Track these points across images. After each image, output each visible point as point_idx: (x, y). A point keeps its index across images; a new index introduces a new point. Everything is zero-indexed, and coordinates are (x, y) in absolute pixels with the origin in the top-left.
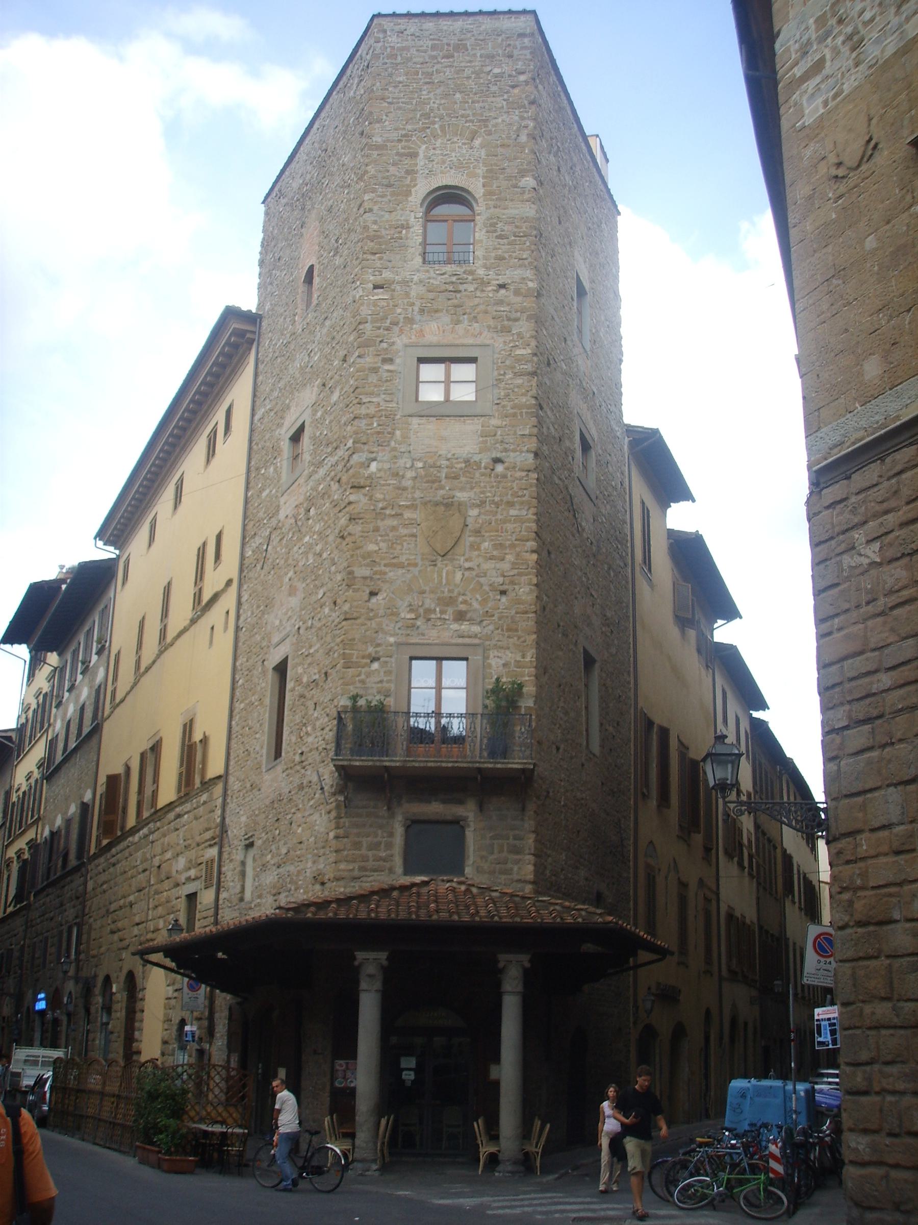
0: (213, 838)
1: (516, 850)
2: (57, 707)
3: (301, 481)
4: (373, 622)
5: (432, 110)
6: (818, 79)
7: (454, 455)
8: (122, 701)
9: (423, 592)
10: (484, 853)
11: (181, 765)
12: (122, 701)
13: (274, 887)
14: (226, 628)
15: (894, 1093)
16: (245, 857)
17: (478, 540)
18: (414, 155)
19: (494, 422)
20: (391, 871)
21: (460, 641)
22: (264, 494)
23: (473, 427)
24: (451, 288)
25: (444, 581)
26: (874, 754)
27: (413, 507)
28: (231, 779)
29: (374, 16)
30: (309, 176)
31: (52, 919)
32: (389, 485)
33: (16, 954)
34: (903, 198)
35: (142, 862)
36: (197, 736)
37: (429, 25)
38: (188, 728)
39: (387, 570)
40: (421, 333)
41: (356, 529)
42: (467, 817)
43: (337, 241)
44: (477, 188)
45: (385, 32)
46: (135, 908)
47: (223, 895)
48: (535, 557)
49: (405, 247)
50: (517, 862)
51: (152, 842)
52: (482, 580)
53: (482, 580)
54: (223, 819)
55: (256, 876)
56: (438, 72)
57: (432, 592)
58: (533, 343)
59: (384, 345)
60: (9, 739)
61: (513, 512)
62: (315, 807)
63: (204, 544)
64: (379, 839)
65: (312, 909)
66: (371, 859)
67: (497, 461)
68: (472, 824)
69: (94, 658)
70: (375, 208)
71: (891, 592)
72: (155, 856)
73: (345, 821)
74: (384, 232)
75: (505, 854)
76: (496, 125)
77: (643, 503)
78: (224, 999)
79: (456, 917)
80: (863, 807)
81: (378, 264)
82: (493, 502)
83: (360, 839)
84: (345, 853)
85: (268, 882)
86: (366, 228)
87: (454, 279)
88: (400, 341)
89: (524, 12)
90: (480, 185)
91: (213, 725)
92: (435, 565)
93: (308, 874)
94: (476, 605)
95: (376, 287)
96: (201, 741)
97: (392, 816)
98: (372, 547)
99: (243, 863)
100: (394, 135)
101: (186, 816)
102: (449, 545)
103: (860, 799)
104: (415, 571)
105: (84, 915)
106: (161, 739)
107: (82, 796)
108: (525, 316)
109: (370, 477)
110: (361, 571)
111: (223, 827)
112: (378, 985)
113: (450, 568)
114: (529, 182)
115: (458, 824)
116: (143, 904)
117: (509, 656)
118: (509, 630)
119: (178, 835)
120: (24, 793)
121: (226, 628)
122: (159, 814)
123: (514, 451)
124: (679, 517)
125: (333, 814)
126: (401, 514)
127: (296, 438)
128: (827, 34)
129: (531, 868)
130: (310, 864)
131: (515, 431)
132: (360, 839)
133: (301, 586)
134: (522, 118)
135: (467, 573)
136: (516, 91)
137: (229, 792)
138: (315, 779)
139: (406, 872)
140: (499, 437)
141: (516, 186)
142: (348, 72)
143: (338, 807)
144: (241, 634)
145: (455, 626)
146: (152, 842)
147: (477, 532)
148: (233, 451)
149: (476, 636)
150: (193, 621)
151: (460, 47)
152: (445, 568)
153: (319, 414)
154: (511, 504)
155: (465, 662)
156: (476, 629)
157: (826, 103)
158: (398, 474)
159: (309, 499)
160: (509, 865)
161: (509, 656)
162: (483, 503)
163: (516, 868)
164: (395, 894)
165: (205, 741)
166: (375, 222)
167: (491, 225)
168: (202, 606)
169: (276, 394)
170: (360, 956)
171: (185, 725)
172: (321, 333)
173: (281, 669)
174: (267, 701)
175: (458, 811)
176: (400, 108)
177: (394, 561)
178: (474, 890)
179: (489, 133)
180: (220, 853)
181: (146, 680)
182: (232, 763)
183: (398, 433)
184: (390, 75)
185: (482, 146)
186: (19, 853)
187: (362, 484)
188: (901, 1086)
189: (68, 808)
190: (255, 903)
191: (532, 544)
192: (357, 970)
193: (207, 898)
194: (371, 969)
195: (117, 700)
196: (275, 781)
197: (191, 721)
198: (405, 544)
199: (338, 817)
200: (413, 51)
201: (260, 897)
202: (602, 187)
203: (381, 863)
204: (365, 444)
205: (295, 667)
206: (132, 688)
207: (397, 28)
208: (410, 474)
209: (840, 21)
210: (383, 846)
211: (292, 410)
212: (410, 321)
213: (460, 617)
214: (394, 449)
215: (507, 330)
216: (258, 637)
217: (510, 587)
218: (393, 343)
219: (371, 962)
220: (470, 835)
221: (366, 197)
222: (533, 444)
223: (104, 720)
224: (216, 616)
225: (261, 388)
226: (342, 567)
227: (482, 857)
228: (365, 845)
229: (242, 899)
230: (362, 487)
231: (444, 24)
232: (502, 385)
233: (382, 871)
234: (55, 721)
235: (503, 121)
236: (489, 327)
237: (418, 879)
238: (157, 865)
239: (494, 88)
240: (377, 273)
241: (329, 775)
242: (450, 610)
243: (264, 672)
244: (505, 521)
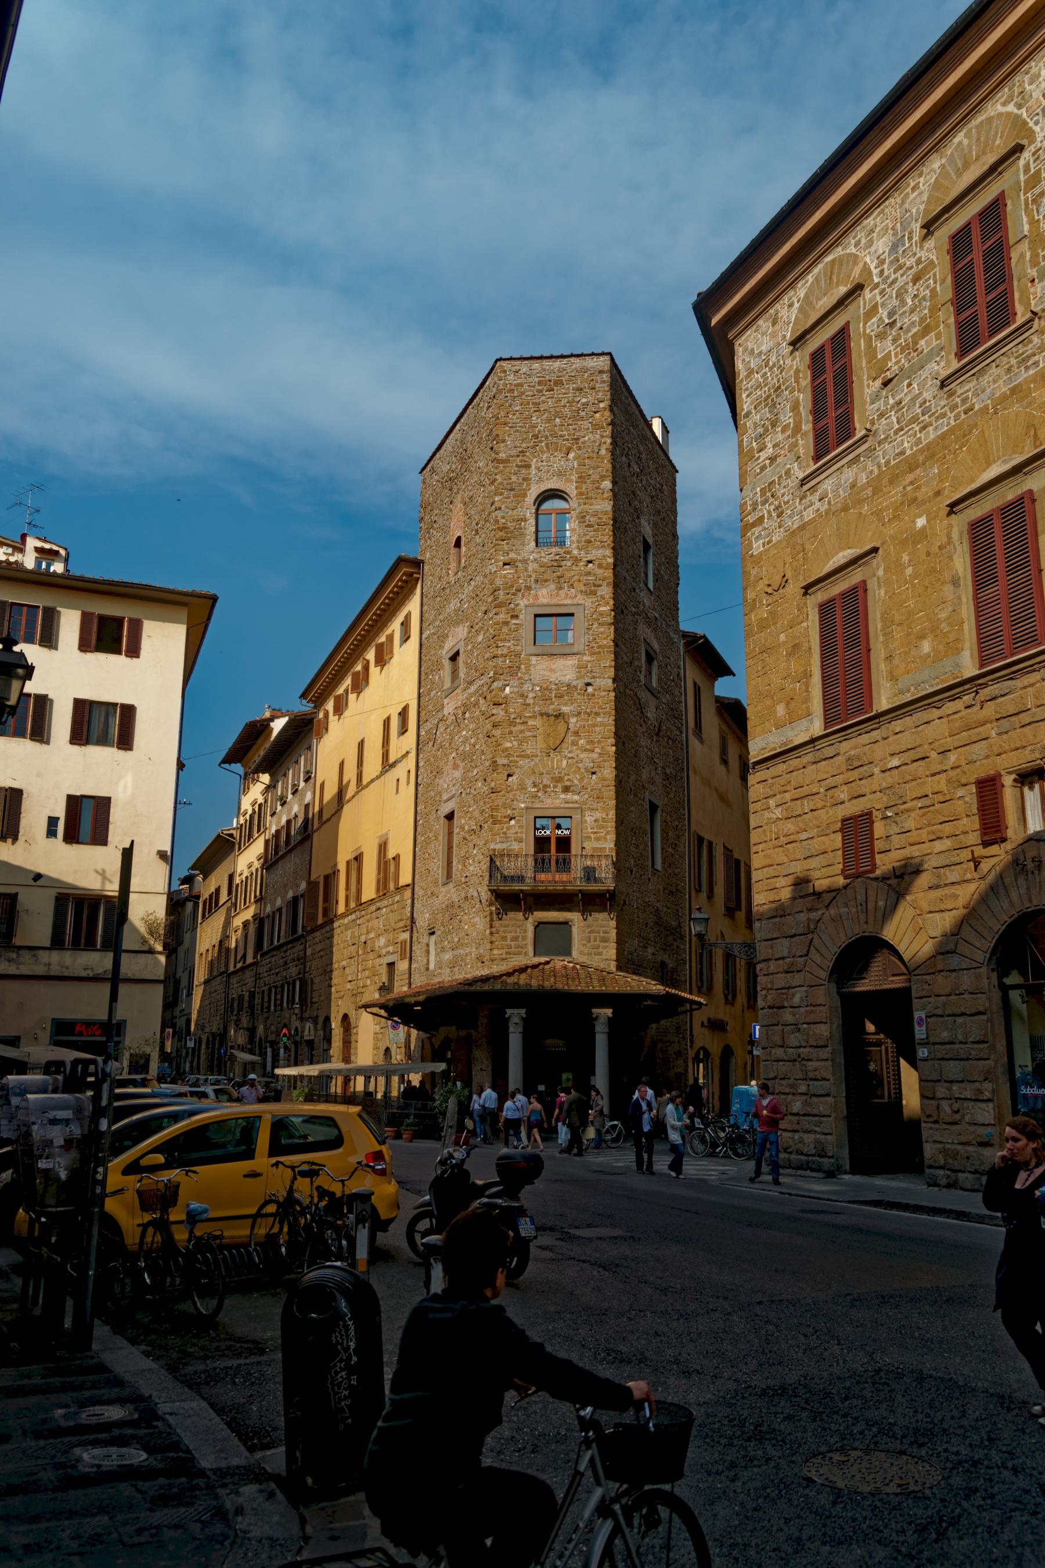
1: (605, 940)
2: (272, 815)
3: (459, 691)
6: (760, 528)
8: (328, 820)
9: (542, 774)
11: (379, 873)
12: (328, 820)
14: (408, 783)
15: (784, 1094)
17: (577, 738)
18: (528, 466)
19: (586, 658)
20: (526, 954)
21: (567, 805)
22: (433, 693)
23: (571, 661)
26: (777, 920)
27: (534, 717)
28: (417, 888)
29: (497, 360)
30: (454, 466)
31: (277, 974)
33: (246, 998)
34: (798, 616)
36: (391, 855)
37: (536, 365)
38: (383, 847)
40: (536, 597)
41: (497, 732)
43: (477, 524)
44: (571, 490)
45: (505, 372)
46: (347, 971)
47: (413, 966)
48: (614, 748)
49: (523, 535)
50: (605, 947)
52: (580, 765)
53: (580, 765)
55: (437, 955)
56: (543, 402)
57: (547, 773)
58: (612, 602)
59: (512, 606)
60: (231, 835)
61: (599, 719)
65: (479, 983)
67: (588, 684)
69: (302, 784)
70: (503, 507)
71: (786, 836)
74: (509, 525)
76: (584, 443)
77: (695, 684)
78: (414, 1032)
79: (566, 987)
80: (772, 947)
81: (506, 548)
82: (586, 713)
86: (497, 521)
88: (523, 603)
89: (603, 354)
90: (574, 487)
91: (402, 846)
94: (576, 782)
95: (505, 564)
96: (394, 859)
98: (508, 745)
99: (428, 945)
100: (514, 452)
102: (558, 742)
103: (770, 943)
104: (537, 760)
105: (305, 972)
107: (298, 886)
108: (605, 583)
109: (506, 697)
110: (501, 761)
112: (520, 1029)
114: (607, 484)
116: (354, 968)
117: (598, 815)
118: (598, 798)
120: (247, 878)
121: (408, 783)
123: (599, 677)
124: (723, 687)
125: (488, 919)
127: (454, 658)
128: (767, 501)
129: (615, 951)
133: (462, 765)
134: (602, 436)
136: (598, 415)
138: (475, 894)
139: (535, 955)
140: (589, 668)
141: (598, 488)
142: (480, 395)
143: (491, 914)
144: (420, 788)
145: (563, 796)
147: (576, 733)
148: (405, 657)
150: (382, 773)
151: (559, 383)
152: (556, 757)
153: (469, 647)
154: (597, 714)
156: (576, 797)
157: (764, 544)
159: (464, 705)
161: (598, 815)
162: (579, 713)
163: (604, 951)
164: (529, 970)
165: (396, 858)
166: (503, 517)
168: (388, 765)
169: (437, 623)
170: (509, 1011)
171: (380, 846)
172: (468, 589)
174: (441, 838)
176: (517, 431)
178: (578, 967)
179: (580, 449)
181: (324, 827)
182: (417, 877)
184: (510, 406)
185: (575, 458)
186: (246, 924)
188: (787, 1090)
189: (287, 893)
191: (612, 741)
192: (507, 1020)
193: (402, 966)
194: (516, 1020)
195: (324, 819)
196: (449, 893)
197: (385, 843)
199: (492, 920)
200: (526, 387)
201: (441, 968)
202: (664, 457)
205: (460, 818)
207: (514, 369)
208: (531, 695)
209: (773, 496)
211: (450, 638)
212: (529, 588)
213: (566, 789)
214: (520, 678)
215: (593, 593)
216: (432, 794)
217: (597, 770)
219: (516, 1016)
221: (496, 499)
222: (612, 674)
223: (313, 832)
224: (400, 771)
225: (426, 615)
226: (488, 757)
229: (427, 969)
231: (546, 363)
232: (591, 632)
234: (270, 825)
236: (581, 591)
237: (543, 959)
239: (583, 414)
241: (485, 895)
242: (560, 785)
243: (438, 818)
244: (594, 725)
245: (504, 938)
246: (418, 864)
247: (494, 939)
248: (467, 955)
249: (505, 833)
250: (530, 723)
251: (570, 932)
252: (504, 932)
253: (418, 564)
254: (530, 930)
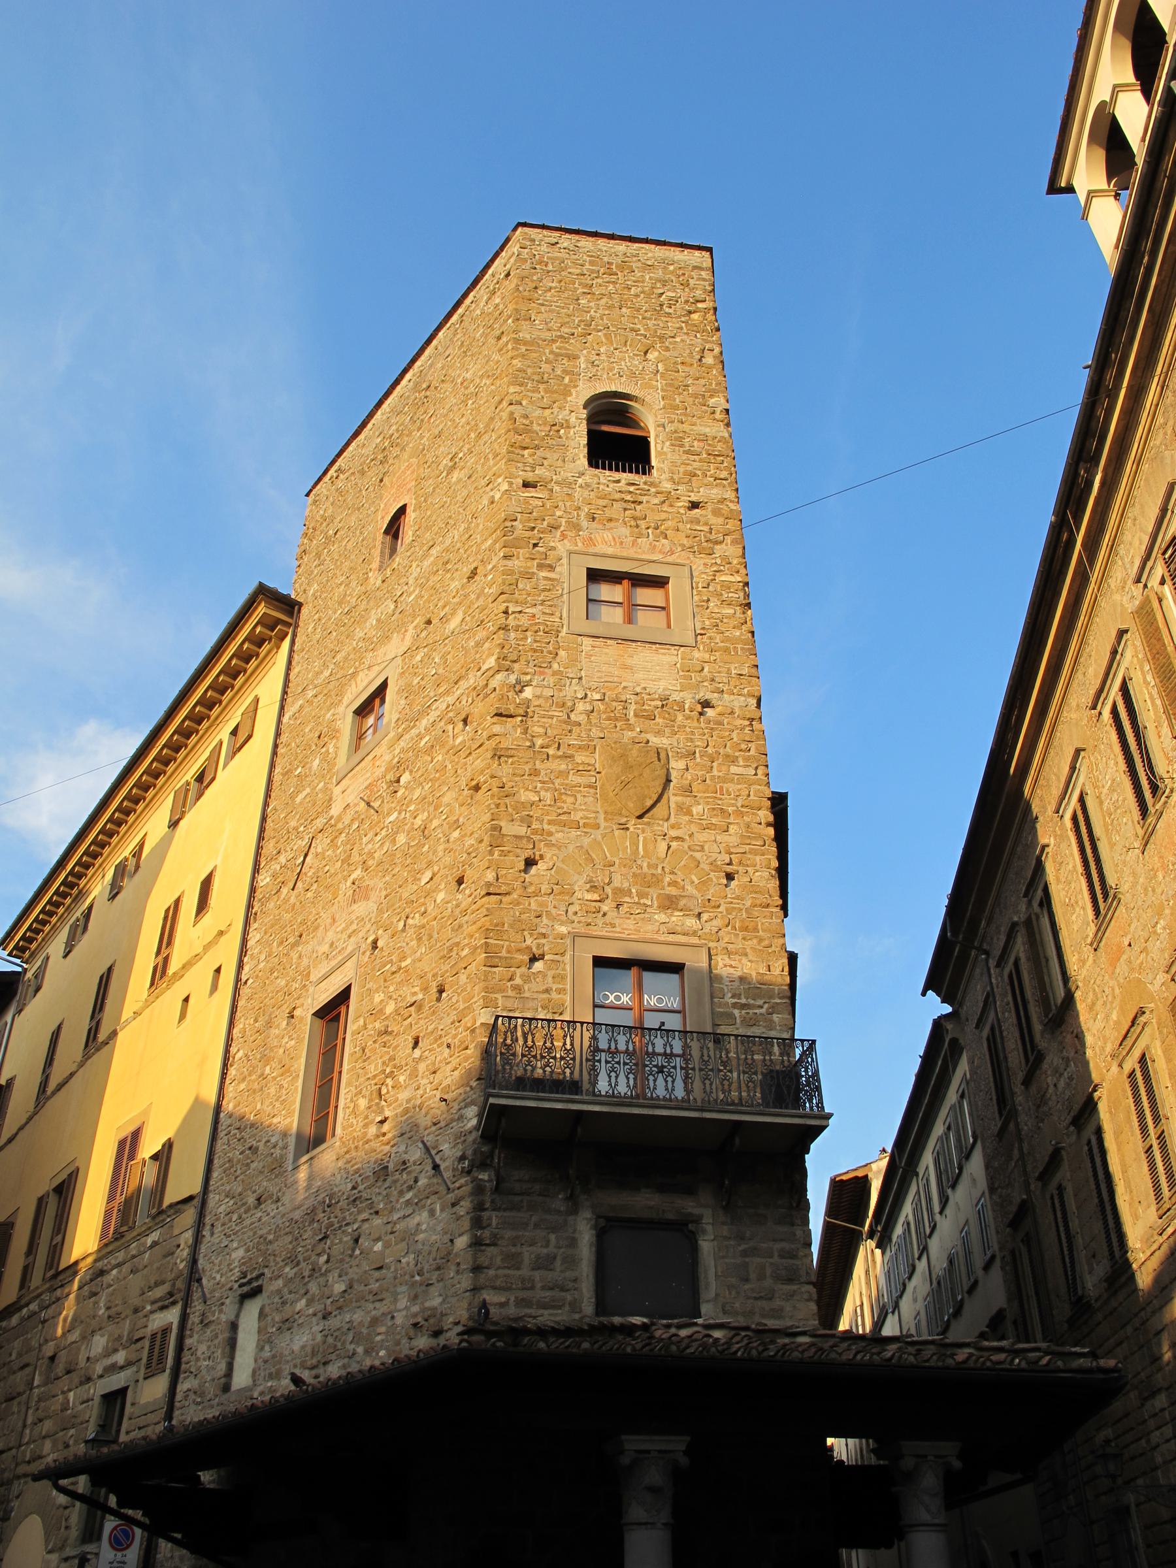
0: (171, 1294)
4: (532, 900)
5: (592, 319)
7: (645, 688)
10: (733, 1280)
13: (314, 1353)
16: (237, 1316)
21: (671, 938)
23: (669, 657)
24: (628, 498)
27: (590, 748)
28: (213, 1199)
32: (552, 717)
35: (20, 1355)
37: (586, 243)
39: (553, 829)
41: (505, 770)
42: (700, 1217)
47: (182, 1387)
50: (790, 1296)
51: (45, 1321)
53: (698, 855)
54: (194, 1261)
61: (734, 769)
62: (417, 1205)
63: (177, 902)
64: (551, 1249)
66: (539, 1285)
68: (709, 1228)
72: (46, 1341)
73: (494, 1218)
74: (535, 427)
75: (768, 1282)
83: (518, 1249)
84: (492, 1272)
85: (296, 1348)
87: (632, 489)
88: (562, 548)
92: (627, 829)
93: (399, 1320)
95: (526, 485)
97: (574, 1210)
98: (526, 796)
99: (234, 1327)
101: (114, 1272)
104: (597, 834)
106: (78, 1169)
110: (509, 829)
111: (193, 1275)
115: (685, 1230)
118: (746, 929)
119: (96, 1303)
121: (214, 987)
122: (61, 1277)
125: (466, 1204)
126: (571, 756)
129: (813, 1307)
130: (403, 1303)
131: (729, 669)
132: (518, 1249)
135: (674, 844)
137: (208, 1220)
142: (468, 301)
143: (479, 1189)
145: (662, 917)
146: (45, 1321)
147: (688, 790)
149: (695, 933)
154: (734, 761)
155: (675, 977)
156: (691, 923)
158: (564, 704)
160: (777, 1303)
167: (676, 439)
170: (633, 1443)
171: (122, 1144)
173: (333, 1011)
175: (690, 1206)
177: (563, 817)
179: (667, 349)
180: (184, 1317)
183: (562, 653)
187: (512, 712)
190: (260, 1389)
194: (654, 1476)
198: (578, 796)
199: (479, 1207)
203: (556, 1293)
204: (515, 661)
206: (30, 1119)
210: (558, 1263)
213: (669, 903)
218: (553, 548)
219: (653, 1455)
220: (706, 1246)
227: (730, 1287)
228: (526, 1261)
229: (226, 1388)
230: (511, 716)
233: (560, 1307)
235: (682, 341)
238: (50, 1354)
240: (528, 469)
242: (654, 892)
245: (514, 1261)
246: (220, 1146)
247: (483, 1260)
248: (375, 1322)
249: (518, 989)
250: (579, 758)
251: (695, 1249)
252: (514, 1241)
253: (290, 606)
254: (586, 1237)
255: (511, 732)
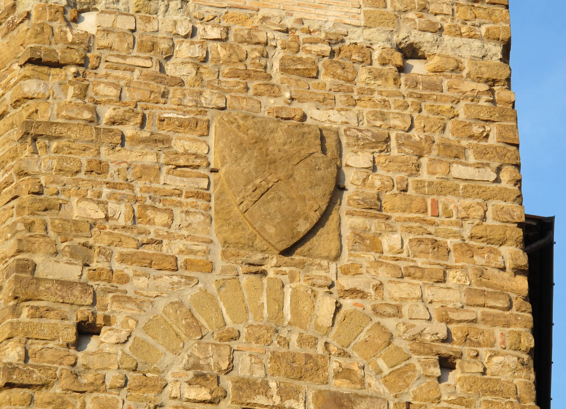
17: (374, 225)
25: (288, 316)
61: (458, 170)
98: (81, 210)
104: (210, 282)
113: (302, 283)
147: (374, 207)
152: (290, 281)
154: (458, 155)
177: (149, 250)
187: (59, 56)
255: (56, 94)
